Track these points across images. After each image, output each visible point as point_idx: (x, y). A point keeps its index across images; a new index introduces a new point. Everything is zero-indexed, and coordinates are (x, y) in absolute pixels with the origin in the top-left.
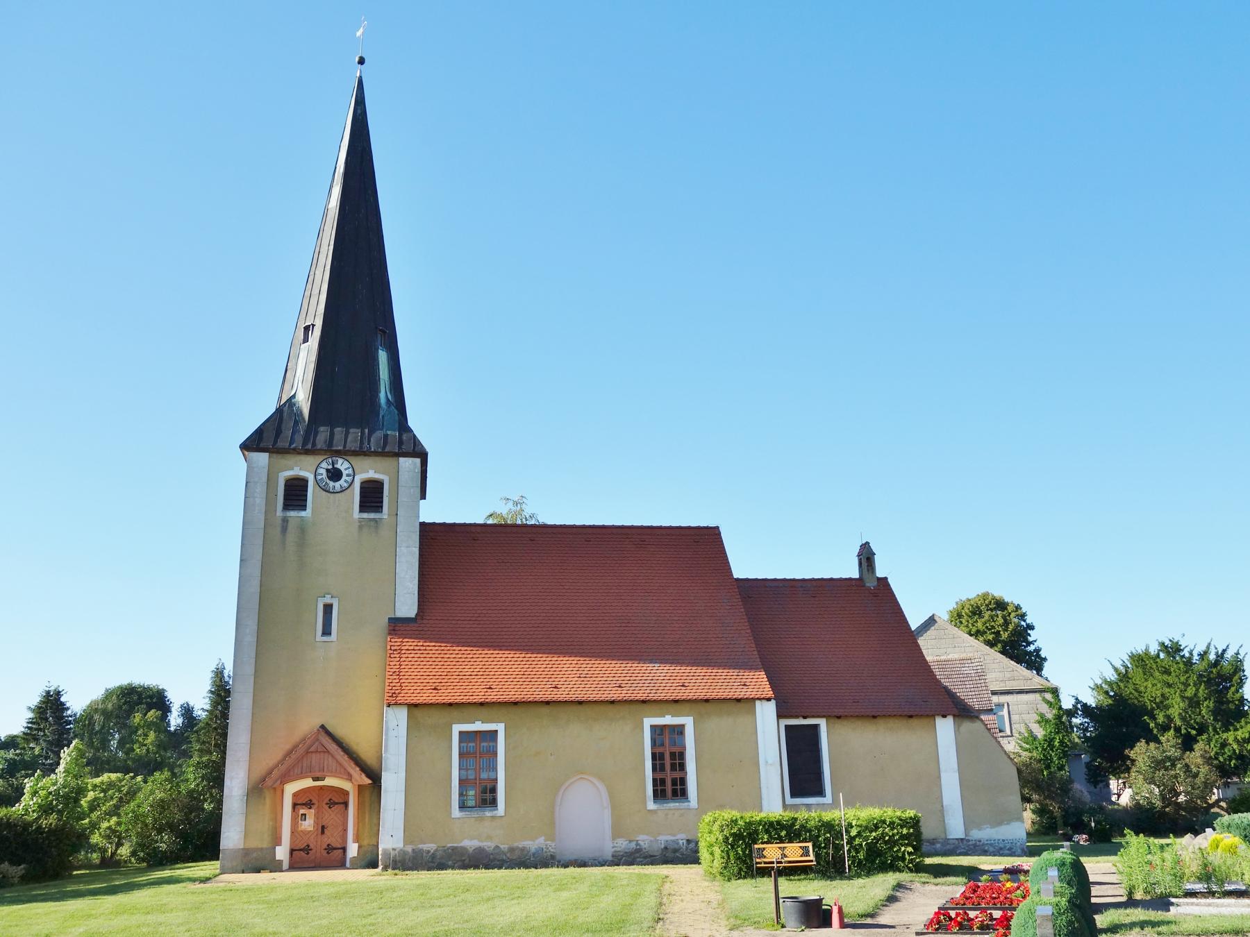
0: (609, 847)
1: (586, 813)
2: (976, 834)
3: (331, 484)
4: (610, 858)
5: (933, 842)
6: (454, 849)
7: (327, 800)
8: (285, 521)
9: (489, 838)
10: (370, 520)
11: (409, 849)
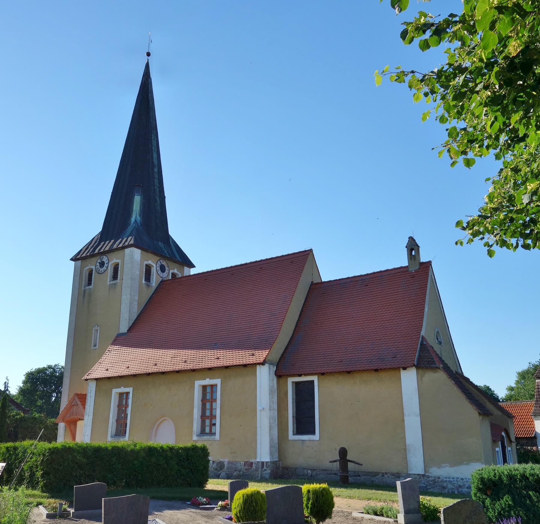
2: (435, 472)
5: (357, 474)
8: (85, 291)
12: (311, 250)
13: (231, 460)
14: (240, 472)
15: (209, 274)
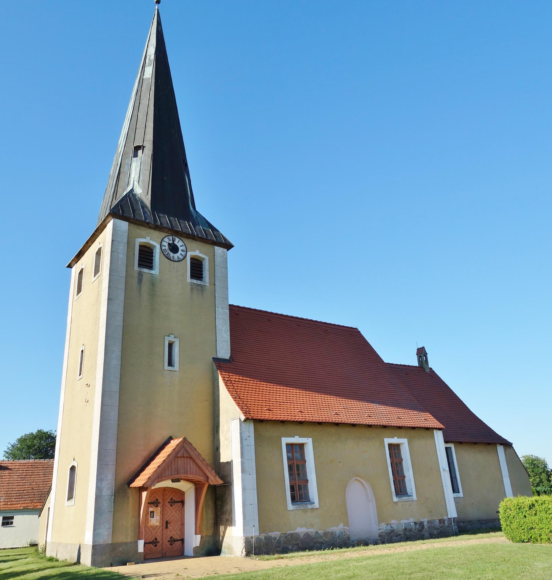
0: (377, 529)
1: (362, 508)
3: (172, 254)
4: (377, 537)
6: (292, 535)
7: (169, 500)
8: (140, 274)
9: (312, 526)
10: (198, 285)
11: (262, 537)
12: (423, 347)
13: (430, 519)
14: (437, 530)
15: (266, 314)
